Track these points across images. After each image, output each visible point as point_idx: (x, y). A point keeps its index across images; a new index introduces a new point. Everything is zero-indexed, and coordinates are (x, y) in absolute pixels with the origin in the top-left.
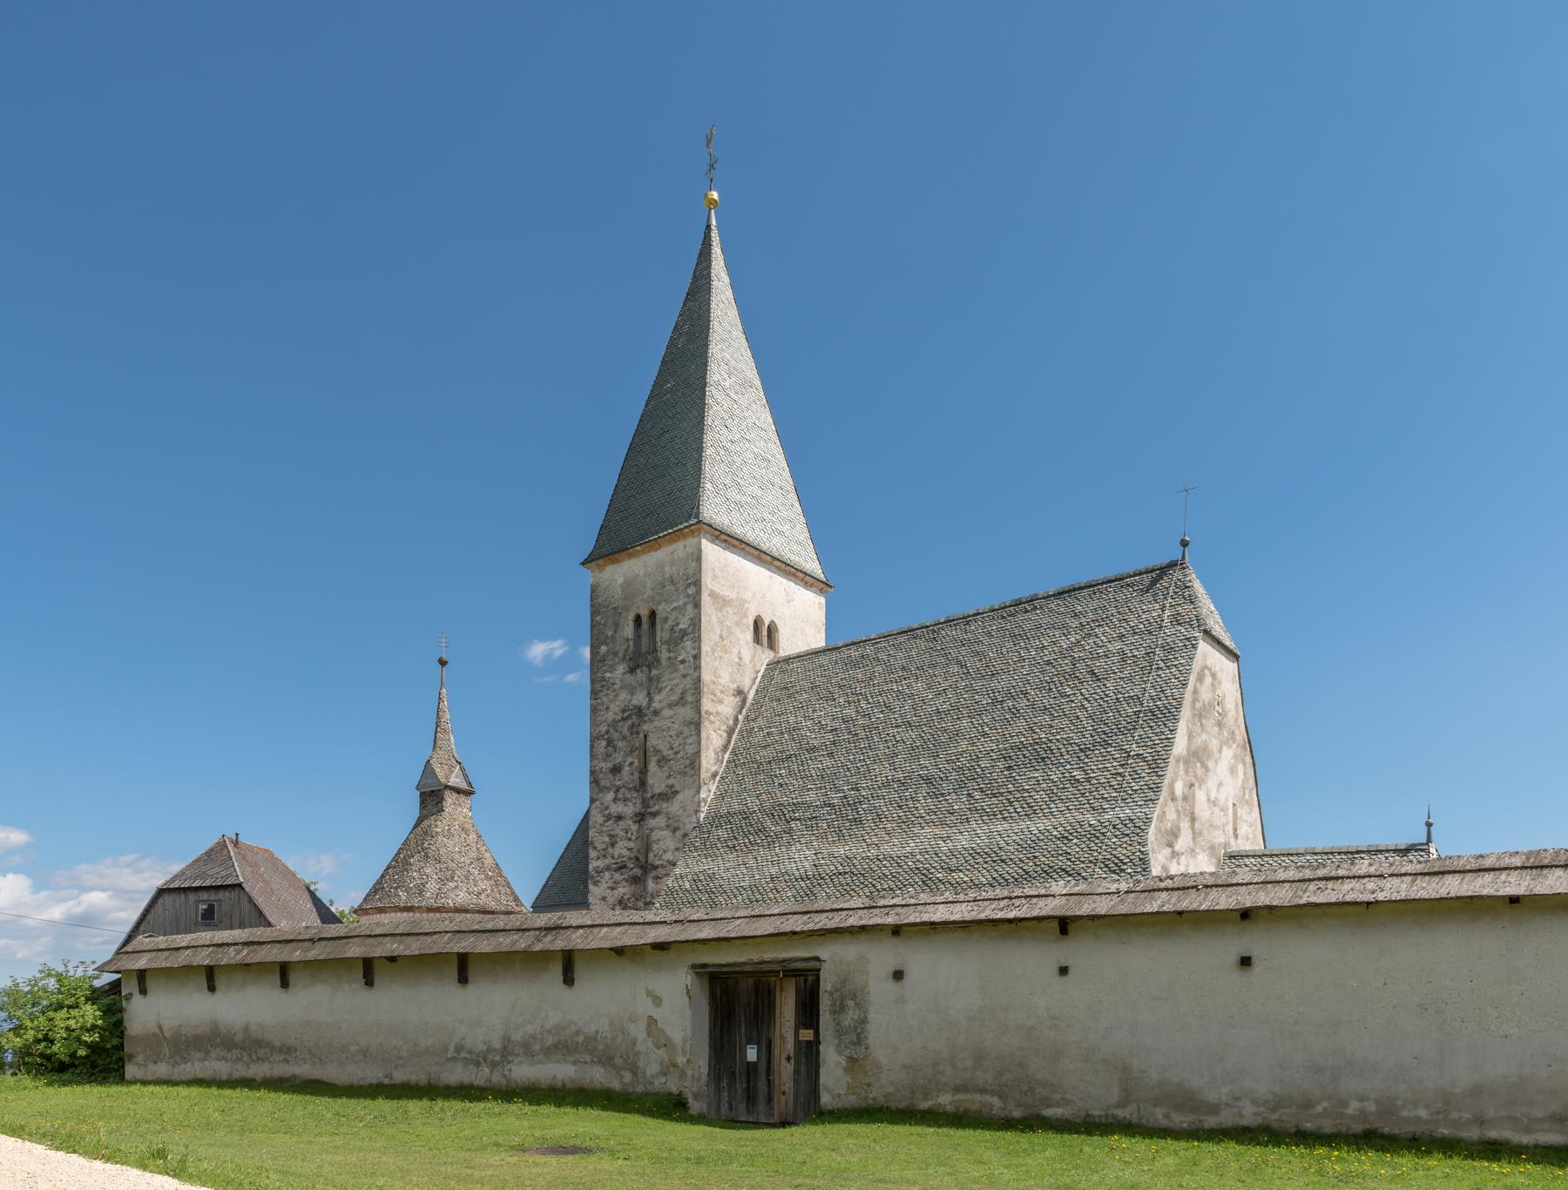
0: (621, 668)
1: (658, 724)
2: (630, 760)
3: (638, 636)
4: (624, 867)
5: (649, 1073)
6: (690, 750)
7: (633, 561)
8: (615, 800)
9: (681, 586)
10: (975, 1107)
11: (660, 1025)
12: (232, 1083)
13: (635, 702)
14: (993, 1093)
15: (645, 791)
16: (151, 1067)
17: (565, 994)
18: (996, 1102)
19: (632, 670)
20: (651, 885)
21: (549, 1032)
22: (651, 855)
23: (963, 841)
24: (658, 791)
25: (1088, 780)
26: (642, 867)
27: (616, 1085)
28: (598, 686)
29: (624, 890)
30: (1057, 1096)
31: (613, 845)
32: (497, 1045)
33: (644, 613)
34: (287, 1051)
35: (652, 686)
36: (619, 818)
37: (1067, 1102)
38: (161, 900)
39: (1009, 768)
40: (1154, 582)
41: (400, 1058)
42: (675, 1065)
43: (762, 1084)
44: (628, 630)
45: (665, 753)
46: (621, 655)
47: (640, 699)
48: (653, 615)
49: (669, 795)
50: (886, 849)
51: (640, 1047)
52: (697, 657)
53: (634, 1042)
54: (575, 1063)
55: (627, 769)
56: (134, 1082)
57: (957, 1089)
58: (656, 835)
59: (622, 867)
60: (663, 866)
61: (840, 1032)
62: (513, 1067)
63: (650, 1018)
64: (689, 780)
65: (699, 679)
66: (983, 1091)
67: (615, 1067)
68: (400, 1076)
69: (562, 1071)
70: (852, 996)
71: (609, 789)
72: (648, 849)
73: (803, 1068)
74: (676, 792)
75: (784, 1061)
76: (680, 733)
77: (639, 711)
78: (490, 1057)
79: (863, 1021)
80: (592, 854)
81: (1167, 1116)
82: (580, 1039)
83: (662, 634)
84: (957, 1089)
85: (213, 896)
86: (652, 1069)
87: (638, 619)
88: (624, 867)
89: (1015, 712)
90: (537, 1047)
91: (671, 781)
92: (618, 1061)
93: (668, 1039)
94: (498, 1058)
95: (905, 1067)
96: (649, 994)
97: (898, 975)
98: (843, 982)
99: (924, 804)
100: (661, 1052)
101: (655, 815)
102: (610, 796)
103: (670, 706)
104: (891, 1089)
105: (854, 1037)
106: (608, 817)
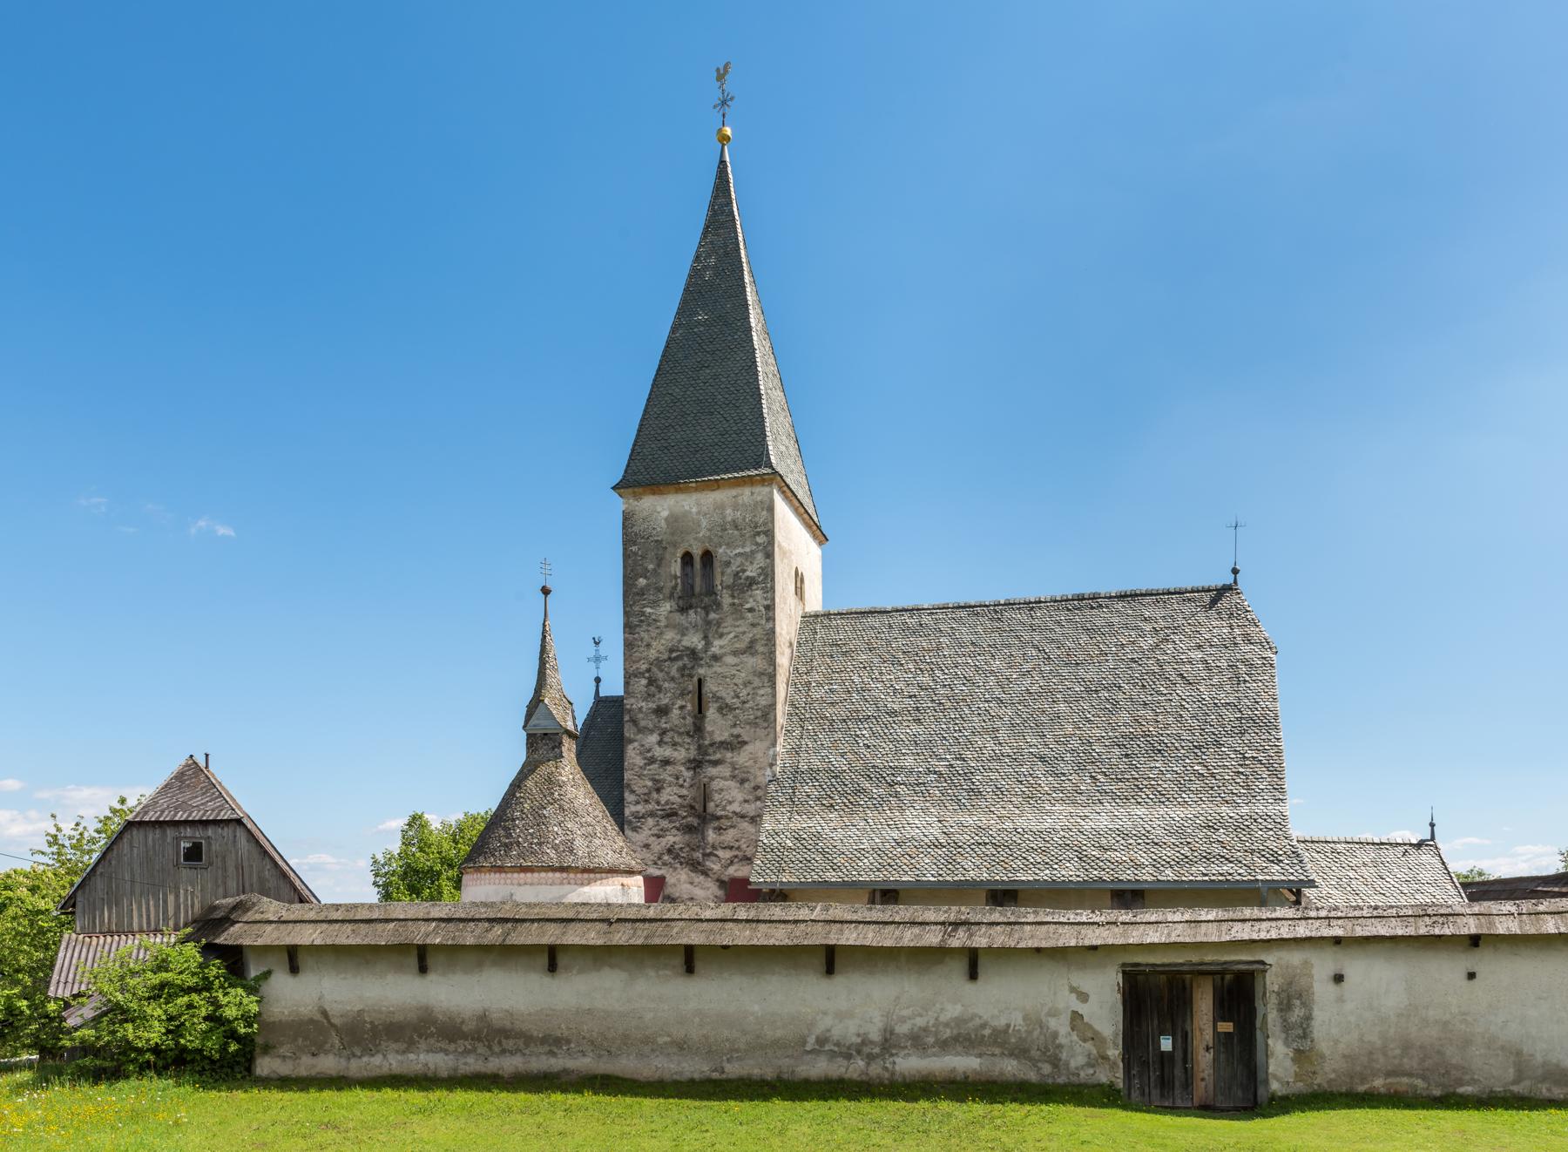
0: (667, 607)
1: (719, 670)
2: (680, 703)
3: (685, 575)
4: (675, 814)
5: (1073, 1064)
6: (763, 702)
7: (680, 497)
8: (660, 743)
9: (748, 532)
10: (1404, 1088)
11: (1086, 1019)
12: (455, 1082)
13: (686, 642)
14: (1418, 1076)
15: (703, 738)
16: (306, 1060)
17: (969, 989)
18: (1419, 1083)
19: (683, 610)
20: (711, 836)
21: (947, 1025)
22: (711, 805)
23: (1103, 822)
24: (718, 739)
25: (1213, 775)
26: (699, 817)
27: (1032, 1076)
28: (635, 620)
29: (674, 838)
30: (1467, 1077)
31: (658, 790)
32: (875, 1036)
33: (697, 552)
34: (553, 1042)
35: (709, 630)
36: (666, 762)
37: (1473, 1081)
38: (127, 836)
39: (1127, 756)
40: (1214, 602)
41: (737, 1051)
42: (1105, 1058)
43: (1178, 1072)
44: (676, 568)
45: (729, 701)
46: (667, 591)
47: (694, 640)
49: (736, 744)
50: (1021, 823)
51: (1062, 1040)
52: (770, 608)
53: (1055, 1035)
54: (980, 1056)
55: (676, 712)
56: (266, 1083)
57: (1388, 1074)
58: (716, 785)
59: (670, 815)
60: (727, 817)
61: (1287, 1028)
62: (898, 1060)
63: (1075, 1013)
64: (761, 732)
65: (773, 631)
66: (1410, 1075)
67: (1031, 1059)
68: (733, 1070)
69: (965, 1063)
70: (1295, 996)
71: (652, 732)
72: (706, 797)
73: (1222, 1056)
74: (745, 743)
75: (1202, 1052)
76: (746, 684)
77: (693, 653)
78: (866, 1050)
79: (1309, 1018)
80: (629, 797)
81: (1549, 1090)
82: (987, 1032)
83: (722, 578)
84: (1388, 1074)
85: (199, 833)
86: (1077, 1061)
87: (687, 558)
88: (675, 814)
89: (1116, 703)
90: (931, 1040)
91: (736, 731)
92: (1035, 1053)
93: (1096, 1033)
94: (877, 1050)
95: (1344, 1056)
96: (1073, 990)
97: (1339, 978)
98: (1290, 983)
99: (1046, 783)
100: (1089, 1045)
101: (716, 763)
102: (654, 738)
103: (735, 653)
104: (1333, 1076)
105: (1300, 1032)
106: (652, 761)
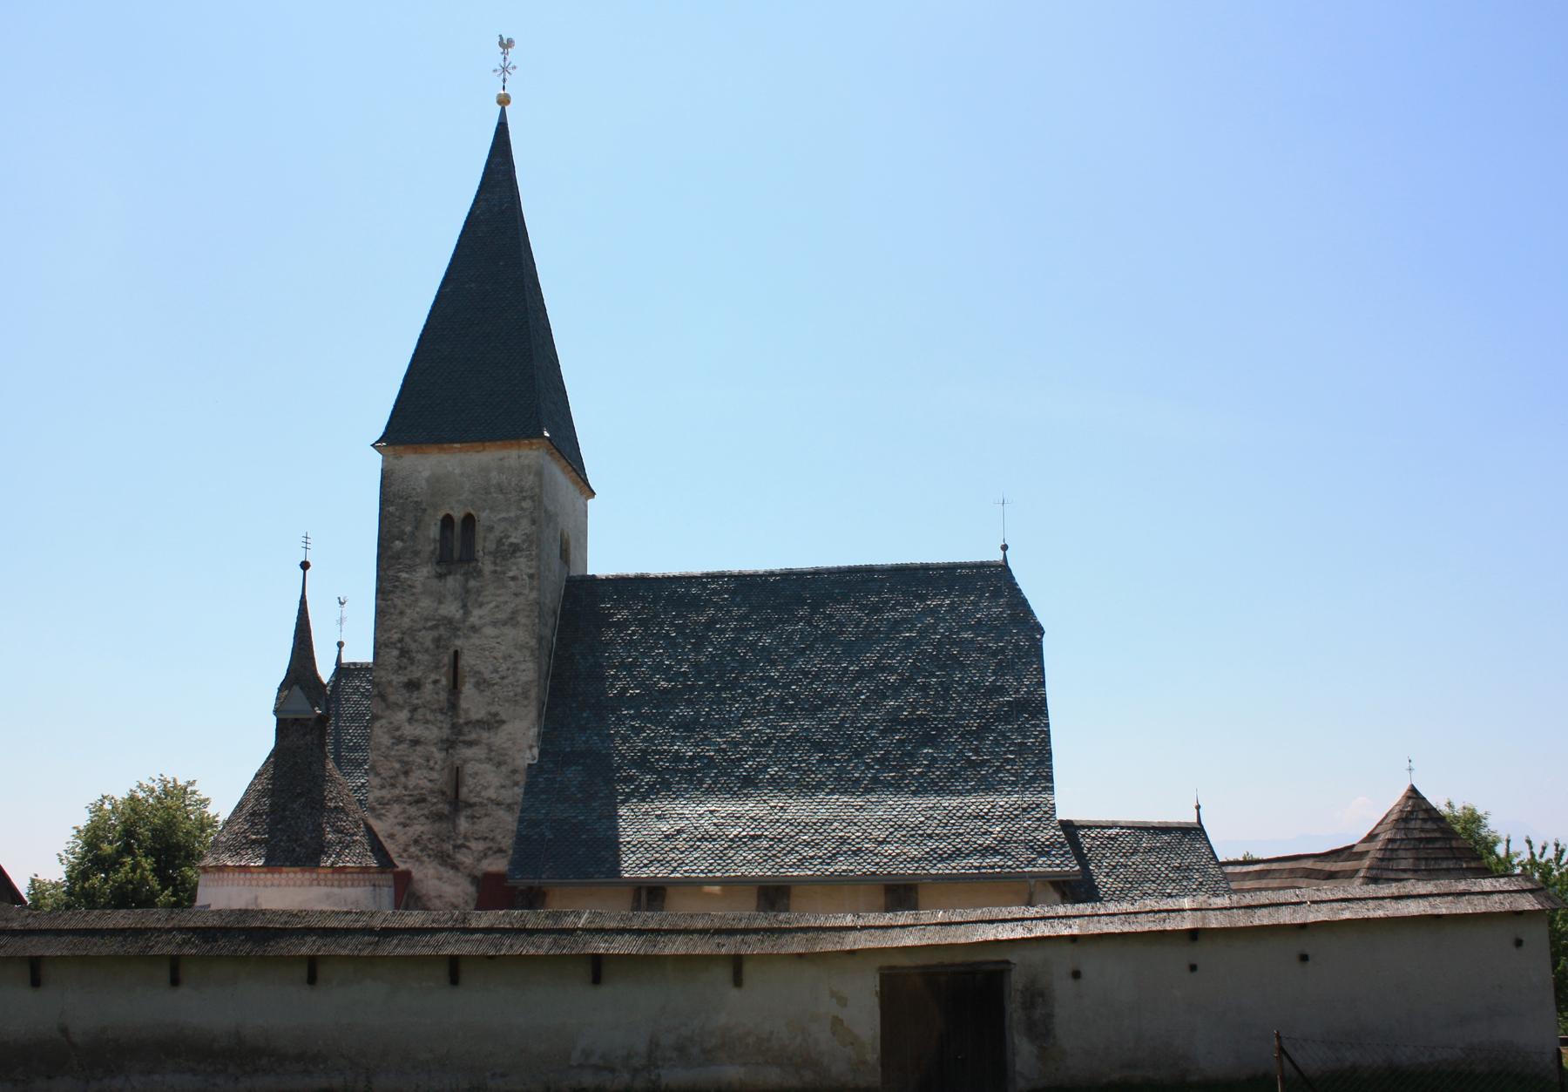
47: (451, 609)
48: (469, 520)
